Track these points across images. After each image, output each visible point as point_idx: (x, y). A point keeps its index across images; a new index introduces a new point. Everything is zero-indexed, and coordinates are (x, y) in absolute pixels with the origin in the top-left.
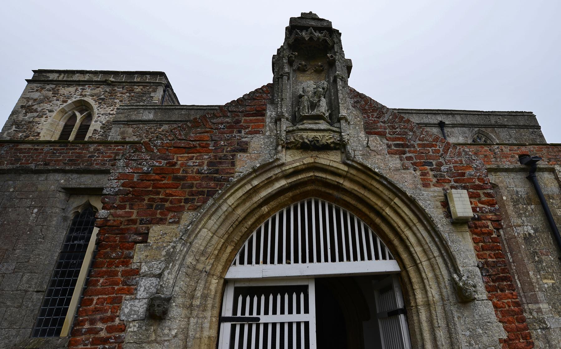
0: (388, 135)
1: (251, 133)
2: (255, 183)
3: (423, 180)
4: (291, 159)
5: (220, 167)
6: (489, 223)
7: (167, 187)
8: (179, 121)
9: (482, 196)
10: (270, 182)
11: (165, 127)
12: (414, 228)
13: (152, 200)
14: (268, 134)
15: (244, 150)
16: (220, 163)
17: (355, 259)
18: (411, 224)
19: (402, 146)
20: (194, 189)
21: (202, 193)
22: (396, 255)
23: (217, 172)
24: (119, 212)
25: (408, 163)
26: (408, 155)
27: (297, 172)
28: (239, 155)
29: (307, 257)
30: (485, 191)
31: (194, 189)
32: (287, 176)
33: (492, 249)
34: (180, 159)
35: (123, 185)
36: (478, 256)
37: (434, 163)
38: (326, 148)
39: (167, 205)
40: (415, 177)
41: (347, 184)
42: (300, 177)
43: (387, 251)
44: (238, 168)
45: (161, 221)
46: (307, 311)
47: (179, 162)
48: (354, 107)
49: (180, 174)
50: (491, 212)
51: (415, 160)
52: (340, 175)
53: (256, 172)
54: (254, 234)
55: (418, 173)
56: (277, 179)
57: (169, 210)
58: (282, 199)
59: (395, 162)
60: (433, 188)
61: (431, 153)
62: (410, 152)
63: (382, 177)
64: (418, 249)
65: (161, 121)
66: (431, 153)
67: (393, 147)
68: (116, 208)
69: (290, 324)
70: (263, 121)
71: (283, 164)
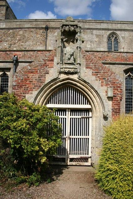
0: (93, 69)
1: (50, 67)
2: (52, 84)
3: (101, 84)
4: (63, 76)
5: (41, 79)
6: (119, 98)
7: (28, 84)
8: (17, 28)
9: (119, 90)
10: (56, 83)
11: (11, 31)
12: (96, 98)
13: (25, 88)
14: (55, 68)
15: (48, 73)
16: (42, 77)
17: (73, 104)
18: (95, 97)
19: (97, 72)
20: (35, 85)
21: (37, 86)
22: (90, 104)
23: (41, 80)
24: (17, 90)
25: (98, 79)
26: (98, 76)
27: (63, 80)
28: (46, 75)
29: (66, 103)
30: (120, 88)
31: (35, 85)
32: (61, 82)
33: (117, 105)
34: (30, 75)
35: (17, 83)
36: (112, 107)
37: (106, 78)
38: (72, 73)
39: (29, 89)
40: (99, 83)
41: (78, 84)
42: (64, 82)
43: (88, 103)
44: (47, 79)
45: (28, 93)
46: (66, 115)
47: (30, 77)
48: (83, 58)
49: (31, 80)
50: (120, 94)
51: (100, 78)
52: (76, 82)
53: (52, 81)
54: (50, 99)
55: (100, 82)
56: (58, 82)
57: (30, 90)
58: (59, 87)
59: (94, 78)
60: (104, 87)
61: (106, 75)
62: (99, 75)
63: (88, 83)
64: (96, 103)
65: (9, 28)
66: (106, 75)
67: (94, 73)
68: (16, 89)
69: (86, 139)
70: (53, 63)
71: (59, 78)
